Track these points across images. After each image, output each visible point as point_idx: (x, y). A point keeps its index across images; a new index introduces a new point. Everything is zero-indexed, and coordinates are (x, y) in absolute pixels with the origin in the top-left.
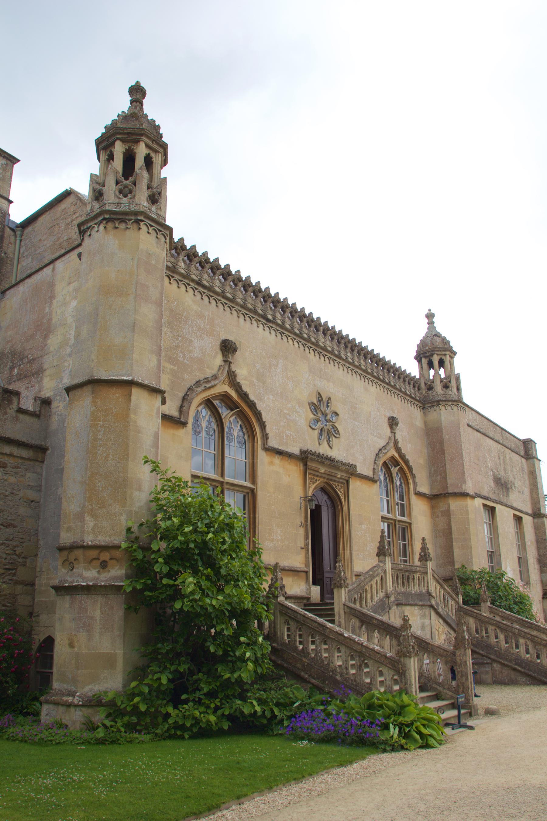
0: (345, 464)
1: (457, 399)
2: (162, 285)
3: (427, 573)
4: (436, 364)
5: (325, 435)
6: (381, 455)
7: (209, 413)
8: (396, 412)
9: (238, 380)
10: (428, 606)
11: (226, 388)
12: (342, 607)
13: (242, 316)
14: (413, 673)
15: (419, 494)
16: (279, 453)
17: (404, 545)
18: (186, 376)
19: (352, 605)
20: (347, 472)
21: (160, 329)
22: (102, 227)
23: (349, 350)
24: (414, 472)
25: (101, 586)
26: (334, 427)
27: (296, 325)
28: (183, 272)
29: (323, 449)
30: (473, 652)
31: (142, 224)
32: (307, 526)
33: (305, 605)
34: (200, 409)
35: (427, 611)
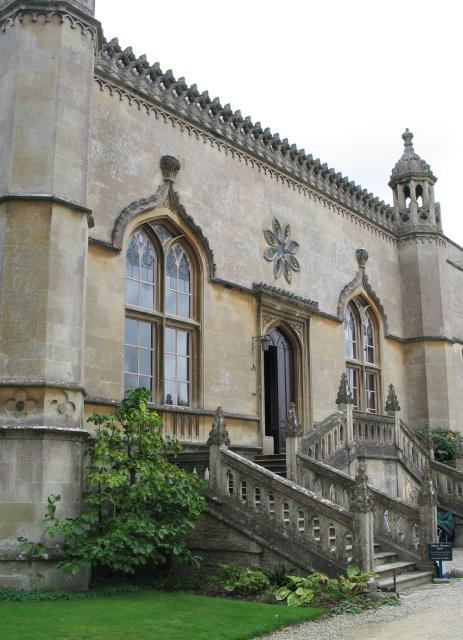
0: (305, 301)
1: (435, 230)
2: (89, 90)
3: (394, 424)
4: (413, 191)
5: (282, 269)
6: (347, 293)
7: (147, 239)
8: (365, 244)
9: (181, 203)
10: (394, 460)
11: (167, 212)
12: (294, 458)
13: (186, 130)
14: (367, 529)
15: (389, 338)
16: (229, 286)
17: (373, 394)
18: (120, 197)
19: (306, 457)
20: (307, 309)
21: (86, 140)
22: (17, 20)
23: (312, 172)
24: (385, 313)
25: (17, 430)
26: (293, 260)
27: (250, 142)
28: (116, 76)
29: (280, 284)
30: (439, 510)
31: (64, 16)
32: (259, 369)
33: (257, 458)
34: (136, 234)
35: (393, 465)
